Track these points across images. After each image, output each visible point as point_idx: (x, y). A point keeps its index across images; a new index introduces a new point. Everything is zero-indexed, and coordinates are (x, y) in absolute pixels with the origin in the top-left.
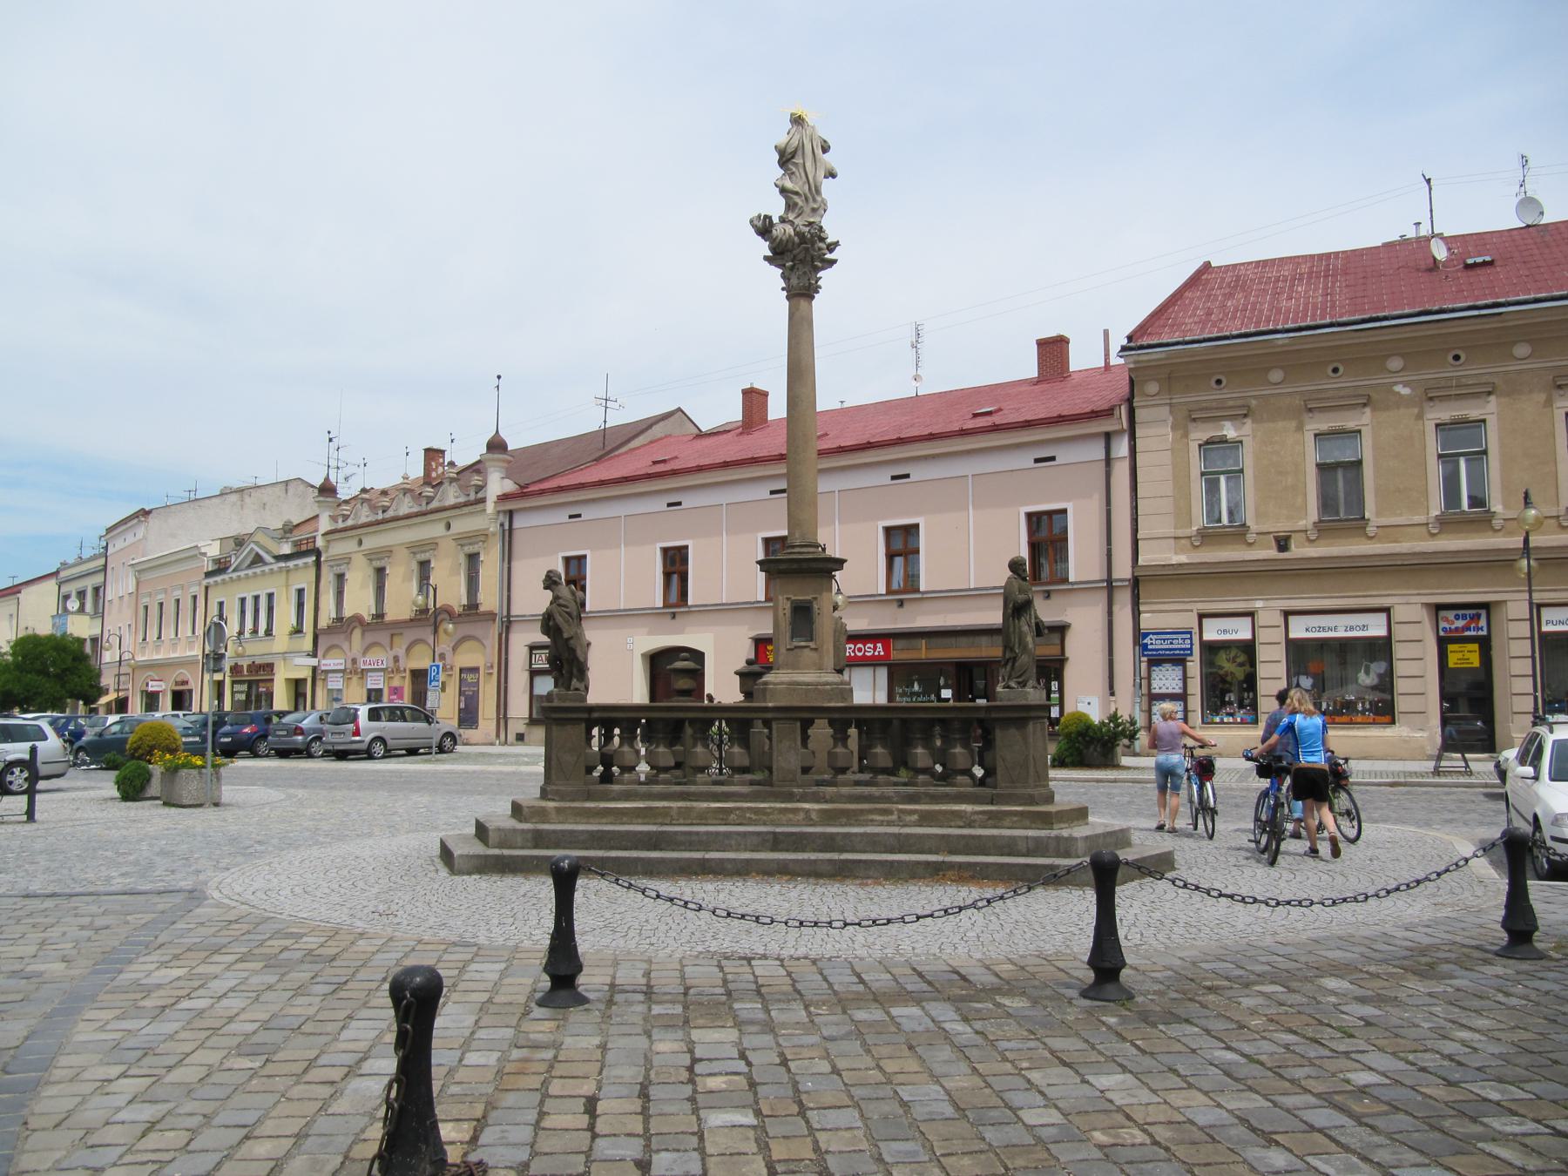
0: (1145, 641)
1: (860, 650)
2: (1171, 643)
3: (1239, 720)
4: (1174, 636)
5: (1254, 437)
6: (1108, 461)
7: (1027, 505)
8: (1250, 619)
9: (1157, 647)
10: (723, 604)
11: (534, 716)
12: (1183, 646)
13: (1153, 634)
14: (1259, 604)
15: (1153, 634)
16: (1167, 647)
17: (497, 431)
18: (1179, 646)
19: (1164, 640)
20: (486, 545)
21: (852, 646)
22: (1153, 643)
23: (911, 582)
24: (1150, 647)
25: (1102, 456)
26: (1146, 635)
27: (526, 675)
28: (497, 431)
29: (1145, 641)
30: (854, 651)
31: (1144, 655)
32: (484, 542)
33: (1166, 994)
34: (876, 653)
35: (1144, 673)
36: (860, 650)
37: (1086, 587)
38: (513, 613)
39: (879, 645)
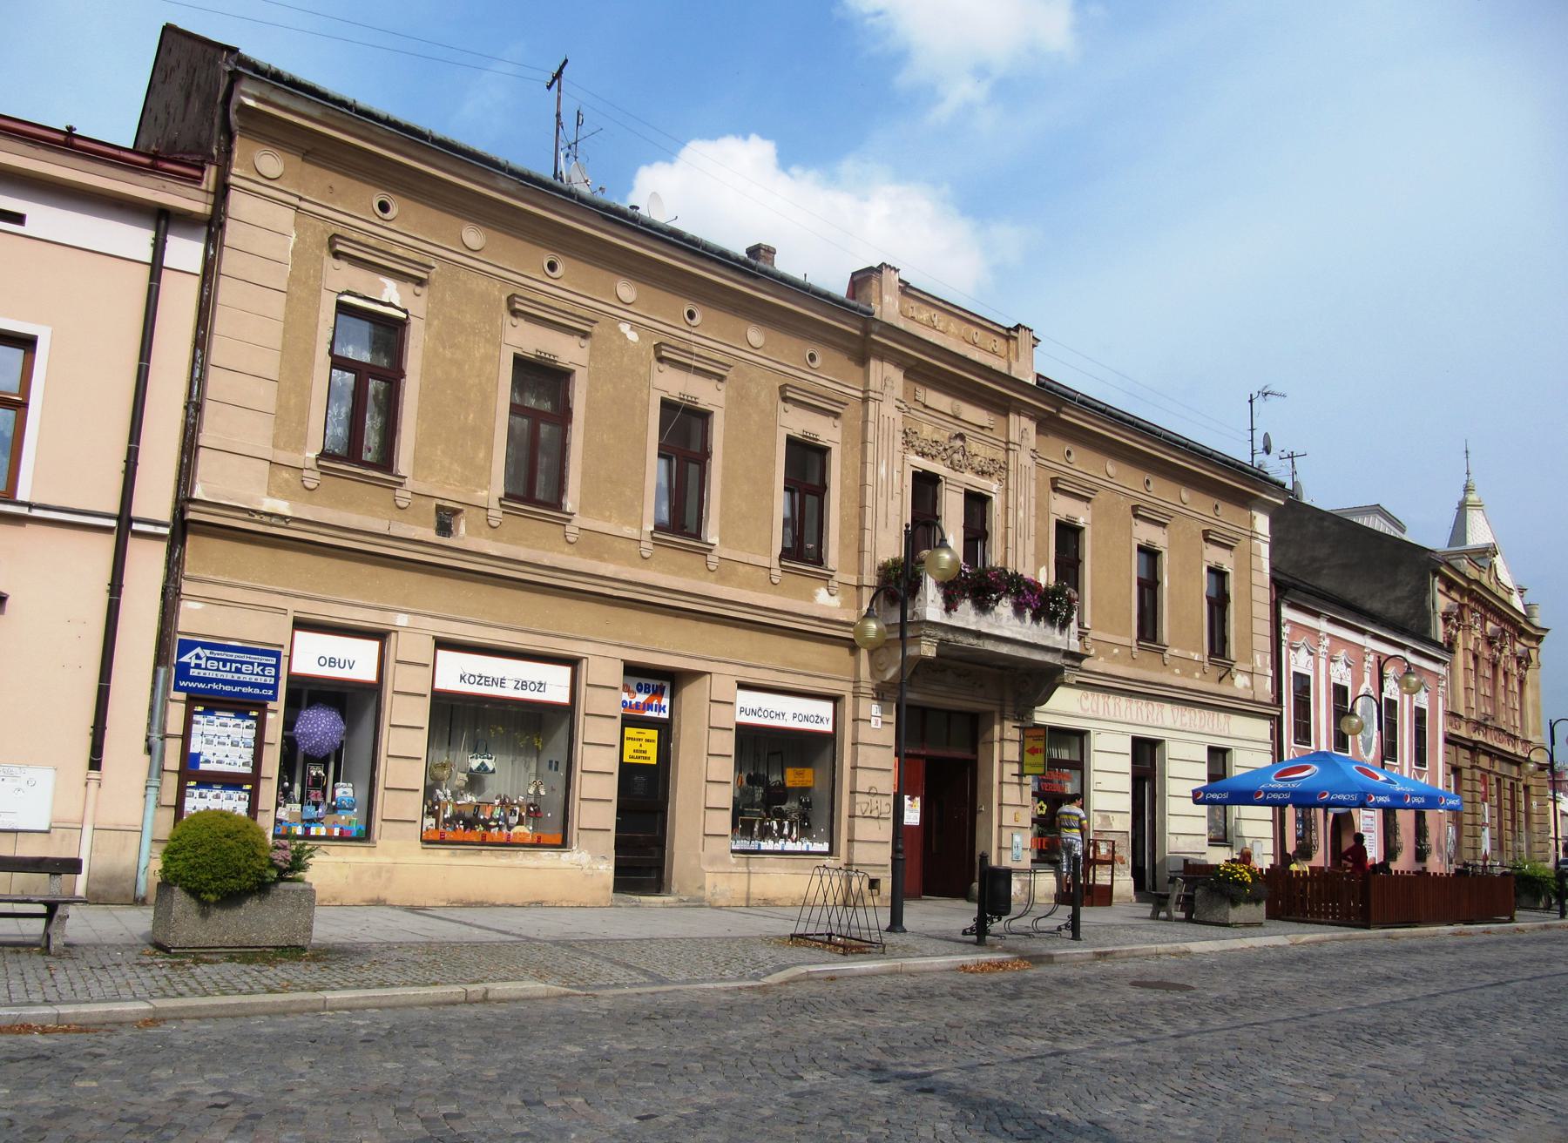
0: (185, 659)
2: (238, 671)
4: (245, 658)
5: (428, 325)
6: (156, 267)
8: (374, 645)
12: (261, 680)
13: (205, 646)
14: (402, 620)
15: (205, 646)
16: (229, 676)
18: (253, 679)
19: (225, 662)
24: (194, 672)
26: (186, 647)
29: (185, 659)
31: (178, 688)
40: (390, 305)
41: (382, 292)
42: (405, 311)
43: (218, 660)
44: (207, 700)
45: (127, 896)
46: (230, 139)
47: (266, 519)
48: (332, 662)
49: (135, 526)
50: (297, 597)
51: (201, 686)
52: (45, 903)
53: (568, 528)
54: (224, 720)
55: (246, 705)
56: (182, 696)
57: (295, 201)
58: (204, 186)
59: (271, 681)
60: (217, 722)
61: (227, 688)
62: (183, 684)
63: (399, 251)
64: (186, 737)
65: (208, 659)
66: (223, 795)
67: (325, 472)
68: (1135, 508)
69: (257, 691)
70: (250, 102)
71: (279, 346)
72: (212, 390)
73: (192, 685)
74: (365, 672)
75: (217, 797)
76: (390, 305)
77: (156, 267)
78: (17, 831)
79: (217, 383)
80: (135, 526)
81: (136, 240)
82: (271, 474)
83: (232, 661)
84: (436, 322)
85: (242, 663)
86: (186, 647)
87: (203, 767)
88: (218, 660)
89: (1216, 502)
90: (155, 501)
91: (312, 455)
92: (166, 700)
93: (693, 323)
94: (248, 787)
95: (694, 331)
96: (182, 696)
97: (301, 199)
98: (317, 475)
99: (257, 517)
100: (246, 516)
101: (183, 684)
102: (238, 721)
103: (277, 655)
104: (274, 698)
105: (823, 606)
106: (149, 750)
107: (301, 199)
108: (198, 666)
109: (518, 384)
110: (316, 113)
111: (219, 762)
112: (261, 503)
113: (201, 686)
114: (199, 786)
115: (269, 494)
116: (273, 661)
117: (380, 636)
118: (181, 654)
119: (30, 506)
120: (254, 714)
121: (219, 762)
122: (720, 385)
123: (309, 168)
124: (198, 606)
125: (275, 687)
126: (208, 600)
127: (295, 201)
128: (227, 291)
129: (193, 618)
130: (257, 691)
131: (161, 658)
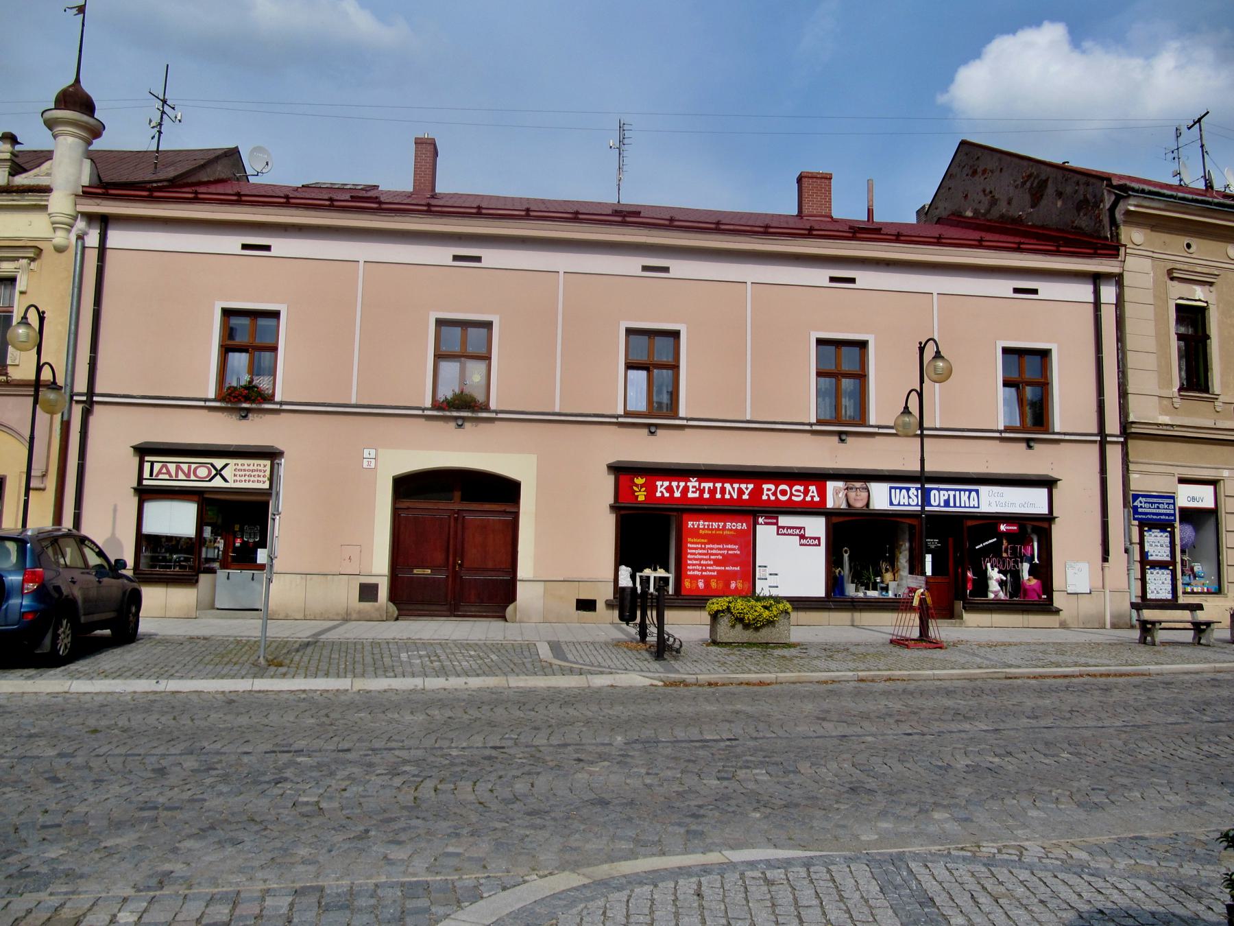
0: (1135, 504)
1: (784, 493)
2: (1158, 508)
3: (1206, 590)
4: (1160, 500)
5: (1218, 307)
6: (1097, 304)
7: (688, 332)
8: (1212, 488)
9: (1148, 511)
10: (936, 429)
11: (142, 567)
12: (1168, 511)
13: (1143, 496)
14: (1226, 473)
15: (1143, 496)
16: (1154, 511)
17: (77, 80)
18: (1165, 511)
19: (1152, 503)
20: (33, 266)
21: (772, 487)
22: (1142, 505)
23: (672, 408)
24: (1140, 510)
25: (1091, 298)
26: (1136, 497)
27: (135, 501)
28: (77, 80)
29: (1135, 504)
30: (775, 494)
31: (1135, 519)
32: (33, 260)
33: (716, 822)
34: (808, 499)
35: (1136, 538)
36: (784, 493)
37: (1077, 439)
38: (98, 390)
39: (813, 488)
40: (1200, 300)
41: (1195, 294)
42: (1206, 302)
43: (1149, 503)
44: (1147, 524)
45: (1127, 624)
46: (1117, 227)
47: (1165, 427)
48: (1194, 499)
49: (1109, 439)
50: (1177, 466)
51: (1144, 517)
52: (938, 645)
53: (1216, 404)
54: (1156, 534)
55: (1164, 525)
56: (1136, 523)
57: (1150, 254)
58: (1120, 259)
59: (1172, 512)
60: (1153, 535)
61: (1155, 517)
62: (1136, 516)
63: (1199, 269)
64: (1142, 543)
65: (1145, 503)
66: (1160, 572)
67: (1183, 398)
68: (1170, 272)
69: (1167, 518)
70: (1132, 208)
71: (1154, 334)
72: (1130, 364)
73: (1140, 517)
74: (1209, 503)
75: (1158, 573)
76: (1200, 300)
77: (1097, 304)
78: (1077, 594)
79: (1132, 359)
80: (1109, 439)
81: (1084, 292)
82: (1160, 403)
83: (1155, 503)
84: (1221, 305)
85: (1159, 503)
86: (1136, 497)
87: (1150, 558)
88: (1149, 503)
89: (1187, 240)
90: (1113, 426)
91: (1176, 389)
92: (1130, 524)
93: (1191, 251)
94: (1171, 568)
95: (1193, 256)
96: (1136, 523)
97: (1153, 252)
98: (1178, 400)
99: (1161, 427)
100: (1156, 427)
101: (1136, 516)
102: (1162, 534)
103: (1173, 498)
104: (1175, 520)
105: (855, 412)
106: (1126, 551)
107: (1153, 252)
108: (1141, 507)
109: (1180, 321)
110: (1161, 205)
111: (1157, 555)
112: (1158, 419)
113: (1144, 517)
114: (1152, 568)
115: (1161, 414)
116: (1172, 501)
117: (1214, 483)
118: (1134, 501)
119: (688, 420)
120: (1169, 529)
121: (1157, 555)
122: (1212, 289)
123: (1154, 234)
124: (1137, 476)
125: (1174, 515)
126: (1141, 472)
127: (1150, 254)
128: (1129, 310)
129: (1139, 483)
130: (1167, 518)
131: (1126, 504)
